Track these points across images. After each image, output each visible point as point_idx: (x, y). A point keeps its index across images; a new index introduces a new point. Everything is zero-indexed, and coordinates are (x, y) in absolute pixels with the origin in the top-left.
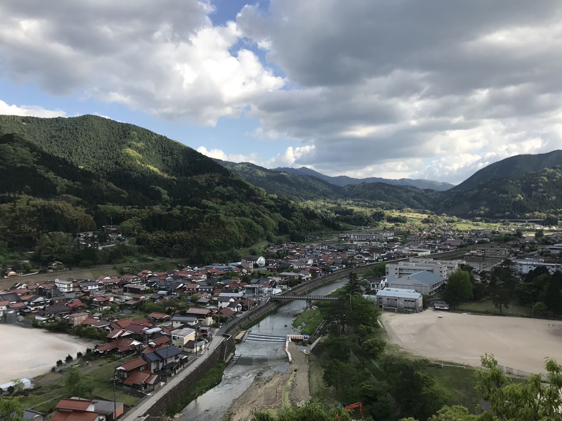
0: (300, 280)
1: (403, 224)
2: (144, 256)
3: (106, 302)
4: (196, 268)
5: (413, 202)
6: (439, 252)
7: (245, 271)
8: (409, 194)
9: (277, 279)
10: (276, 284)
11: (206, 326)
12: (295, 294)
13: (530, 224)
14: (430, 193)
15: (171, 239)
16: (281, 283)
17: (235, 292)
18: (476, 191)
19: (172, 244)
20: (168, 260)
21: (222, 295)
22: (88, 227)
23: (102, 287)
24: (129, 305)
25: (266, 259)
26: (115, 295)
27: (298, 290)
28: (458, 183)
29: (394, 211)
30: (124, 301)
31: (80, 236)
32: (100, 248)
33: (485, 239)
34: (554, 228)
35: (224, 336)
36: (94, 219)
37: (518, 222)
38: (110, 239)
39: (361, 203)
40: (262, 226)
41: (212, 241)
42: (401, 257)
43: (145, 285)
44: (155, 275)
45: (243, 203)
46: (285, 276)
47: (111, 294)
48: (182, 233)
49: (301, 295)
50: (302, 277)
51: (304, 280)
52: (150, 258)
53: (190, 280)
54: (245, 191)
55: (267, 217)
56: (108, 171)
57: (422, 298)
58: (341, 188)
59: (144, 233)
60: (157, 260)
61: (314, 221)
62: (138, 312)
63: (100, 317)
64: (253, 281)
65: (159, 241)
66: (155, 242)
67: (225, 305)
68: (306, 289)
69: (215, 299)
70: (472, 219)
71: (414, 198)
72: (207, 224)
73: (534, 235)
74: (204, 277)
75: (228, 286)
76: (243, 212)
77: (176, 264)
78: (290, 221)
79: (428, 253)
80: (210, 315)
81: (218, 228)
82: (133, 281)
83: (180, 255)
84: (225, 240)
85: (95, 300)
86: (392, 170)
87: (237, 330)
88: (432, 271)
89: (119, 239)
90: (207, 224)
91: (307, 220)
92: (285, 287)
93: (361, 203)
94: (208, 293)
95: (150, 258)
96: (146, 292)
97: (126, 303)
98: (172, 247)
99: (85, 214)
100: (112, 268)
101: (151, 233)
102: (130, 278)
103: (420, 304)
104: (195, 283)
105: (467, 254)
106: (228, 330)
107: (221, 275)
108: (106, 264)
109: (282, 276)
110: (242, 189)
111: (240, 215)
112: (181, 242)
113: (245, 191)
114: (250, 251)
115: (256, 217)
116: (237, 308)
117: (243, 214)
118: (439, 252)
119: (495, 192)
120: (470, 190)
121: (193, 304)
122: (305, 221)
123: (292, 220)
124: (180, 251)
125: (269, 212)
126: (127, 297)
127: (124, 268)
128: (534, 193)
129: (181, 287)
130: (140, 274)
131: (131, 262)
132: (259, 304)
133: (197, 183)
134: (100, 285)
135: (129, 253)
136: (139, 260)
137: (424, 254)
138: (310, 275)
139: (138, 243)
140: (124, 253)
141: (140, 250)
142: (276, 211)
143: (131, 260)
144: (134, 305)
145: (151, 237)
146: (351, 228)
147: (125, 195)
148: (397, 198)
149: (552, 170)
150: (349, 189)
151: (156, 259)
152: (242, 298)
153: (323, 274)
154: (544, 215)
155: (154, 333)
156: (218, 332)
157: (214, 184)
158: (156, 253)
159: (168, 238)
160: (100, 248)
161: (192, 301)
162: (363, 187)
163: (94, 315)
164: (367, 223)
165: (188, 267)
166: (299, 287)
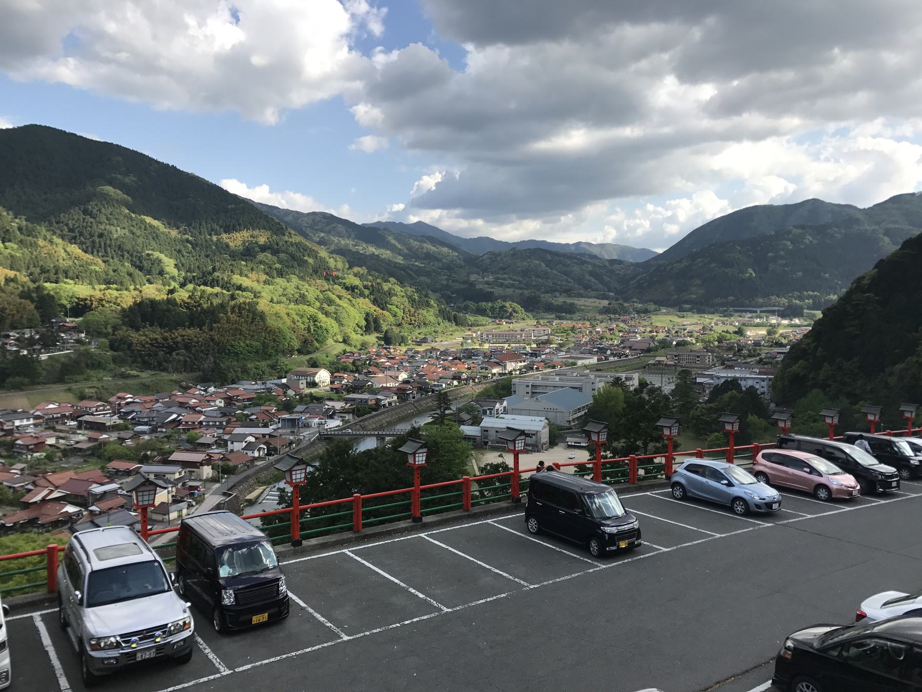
0: (378, 405)
1: (568, 316)
2: (123, 370)
3: (40, 446)
4: (212, 389)
5: (589, 281)
6: (612, 359)
7: (291, 392)
8: (584, 267)
9: (338, 405)
10: (334, 413)
11: (200, 480)
12: (364, 428)
13: (763, 314)
14: (618, 267)
15: (170, 340)
16: (344, 411)
17: (263, 427)
18: (685, 263)
19: (171, 349)
20: (165, 376)
21: (238, 431)
22: (25, 321)
23: (41, 421)
24: (80, 450)
25: (332, 373)
26: (57, 434)
27: (371, 421)
28: (660, 251)
29: (558, 294)
30: (72, 442)
31: (8, 336)
32: (44, 357)
33: (689, 339)
34: (797, 321)
35: (225, 494)
36: (36, 308)
37: (746, 311)
38: (64, 342)
39: (506, 282)
40: (336, 319)
41: (242, 344)
42: (549, 367)
43: (116, 417)
44: (137, 400)
45: (304, 280)
46: (354, 400)
47: (52, 432)
48: (190, 332)
49: (374, 429)
50: (381, 400)
51: (384, 405)
52: (134, 372)
53: (193, 409)
54: (311, 261)
55: (345, 305)
56: (71, 225)
57: (547, 429)
58: (478, 258)
59: (124, 332)
60: (146, 376)
61: (424, 312)
62: (94, 460)
63: (22, 470)
64: (300, 408)
65: (152, 345)
66: (144, 346)
67: (238, 446)
68: (384, 419)
69: (226, 437)
70: (678, 308)
71: (592, 274)
72: (233, 317)
73: (764, 332)
74: (220, 403)
75: (254, 417)
76: (303, 296)
77: (177, 382)
78: (385, 312)
79: (594, 360)
80: (208, 461)
81: (252, 322)
82: (97, 411)
83: (186, 367)
84: (264, 343)
85: (19, 442)
86: (566, 229)
87: (251, 486)
88: (580, 389)
89: (78, 341)
90: (233, 317)
91: (413, 310)
92: (348, 417)
93: (506, 282)
94: (218, 428)
95: (134, 372)
96: (115, 428)
97: (77, 446)
98: (170, 353)
99: (19, 300)
100: (65, 390)
101: (138, 330)
102: (93, 405)
103: (545, 437)
104: (200, 412)
105: (652, 362)
106: (234, 486)
107: (249, 400)
108: (55, 383)
109: (347, 401)
110: (306, 258)
111: (296, 302)
112: (187, 347)
113: (311, 261)
114: (308, 361)
115: (325, 306)
116: (259, 450)
117: (302, 299)
118: (612, 359)
119: (713, 265)
120: (677, 262)
121: (189, 446)
122: (409, 311)
123: (389, 310)
124: (185, 361)
125: (349, 297)
126: (81, 438)
127: (87, 390)
128: (771, 266)
129: (174, 420)
130: (112, 399)
131: (100, 380)
132: (297, 445)
133: (228, 246)
134: (37, 417)
135: (97, 365)
136: (114, 376)
137: (587, 362)
138: (395, 398)
139: (112, 347)
140: (87, 365)
141: (114, 360)
142: (362, 295)
143: (100, 375)
144: (88, 449)
145: (135, 337)
146: (484, 323)
147: (98, 265)
148: (565, 273)
149: (800, 231)
150: (490, 259)
151: (143, 375)
152: (270, 436)
153: (418, 396)
154: (784, 301)
155: (105, 492)
156: (217, 489)
157: (257, 249)
158: (146, 365)
159: (165, 339)
160: (44, 357)
161: (188, 441)
162: (514, 255)
163: (14, 467)
164: (511, 314)
165: (199, 387)
166: (376, 416)
